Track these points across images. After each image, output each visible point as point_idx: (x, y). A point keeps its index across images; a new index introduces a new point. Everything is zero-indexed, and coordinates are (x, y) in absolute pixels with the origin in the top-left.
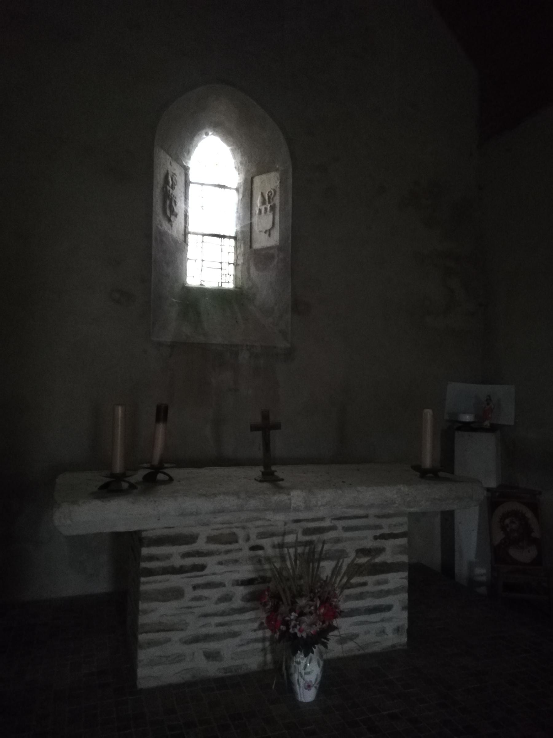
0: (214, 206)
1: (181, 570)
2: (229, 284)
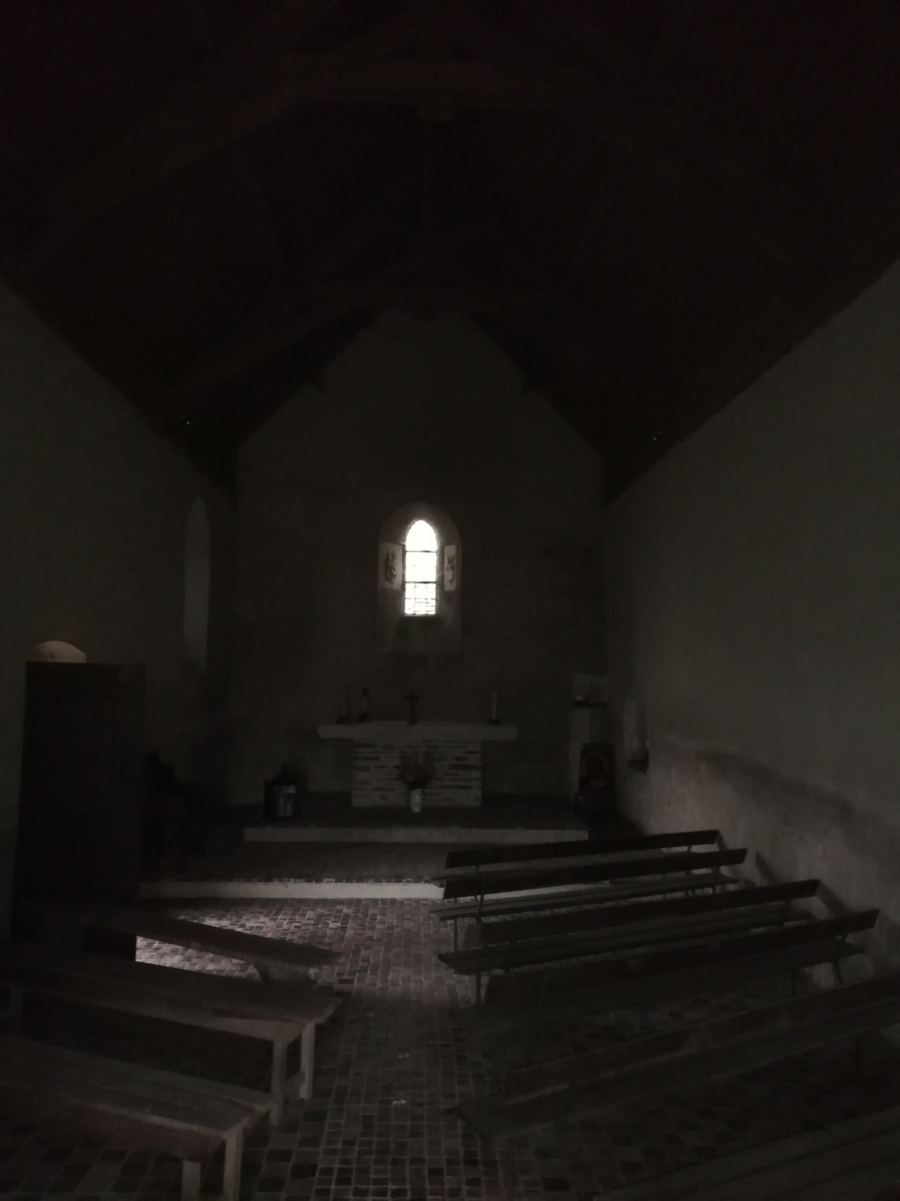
0: (421, 566)
1: (368, 759)
2: (432, 611)
